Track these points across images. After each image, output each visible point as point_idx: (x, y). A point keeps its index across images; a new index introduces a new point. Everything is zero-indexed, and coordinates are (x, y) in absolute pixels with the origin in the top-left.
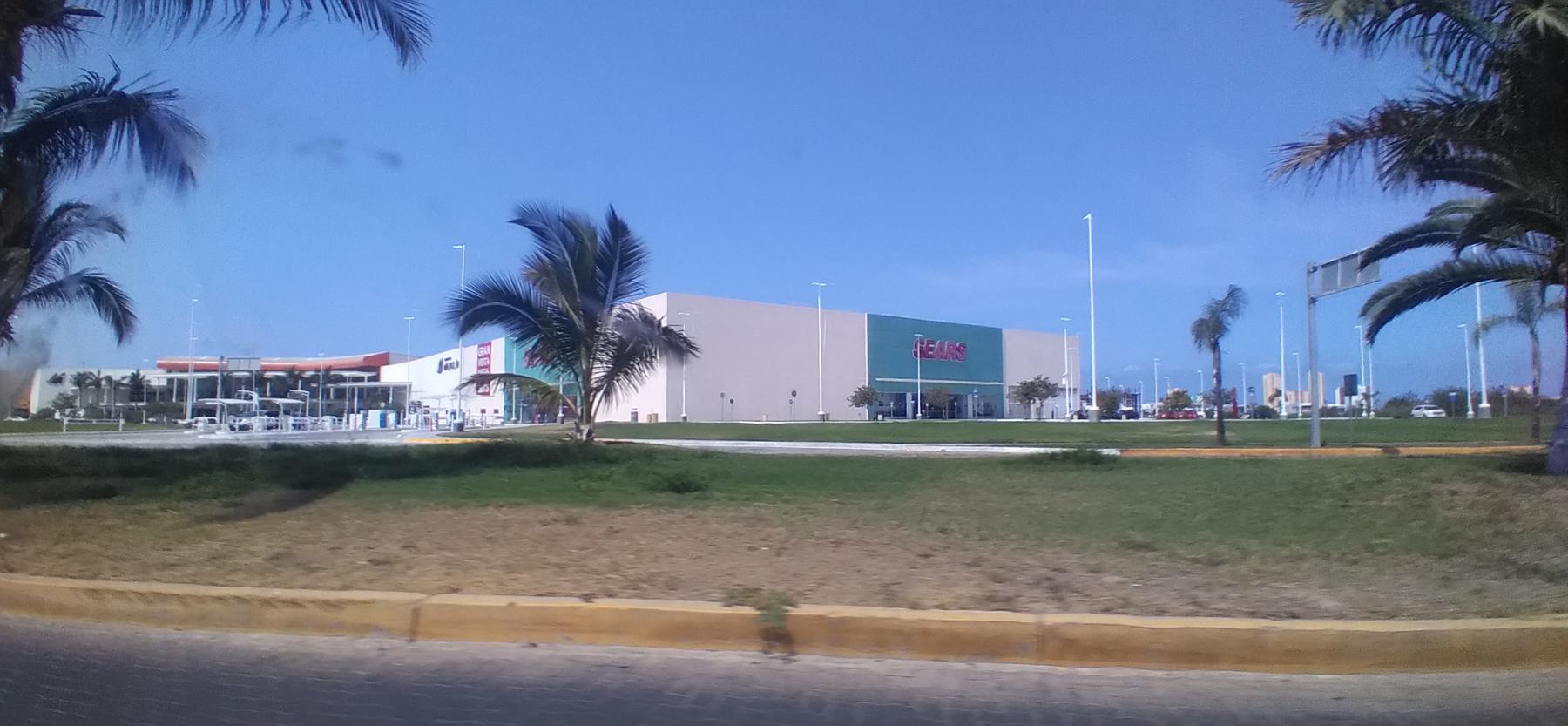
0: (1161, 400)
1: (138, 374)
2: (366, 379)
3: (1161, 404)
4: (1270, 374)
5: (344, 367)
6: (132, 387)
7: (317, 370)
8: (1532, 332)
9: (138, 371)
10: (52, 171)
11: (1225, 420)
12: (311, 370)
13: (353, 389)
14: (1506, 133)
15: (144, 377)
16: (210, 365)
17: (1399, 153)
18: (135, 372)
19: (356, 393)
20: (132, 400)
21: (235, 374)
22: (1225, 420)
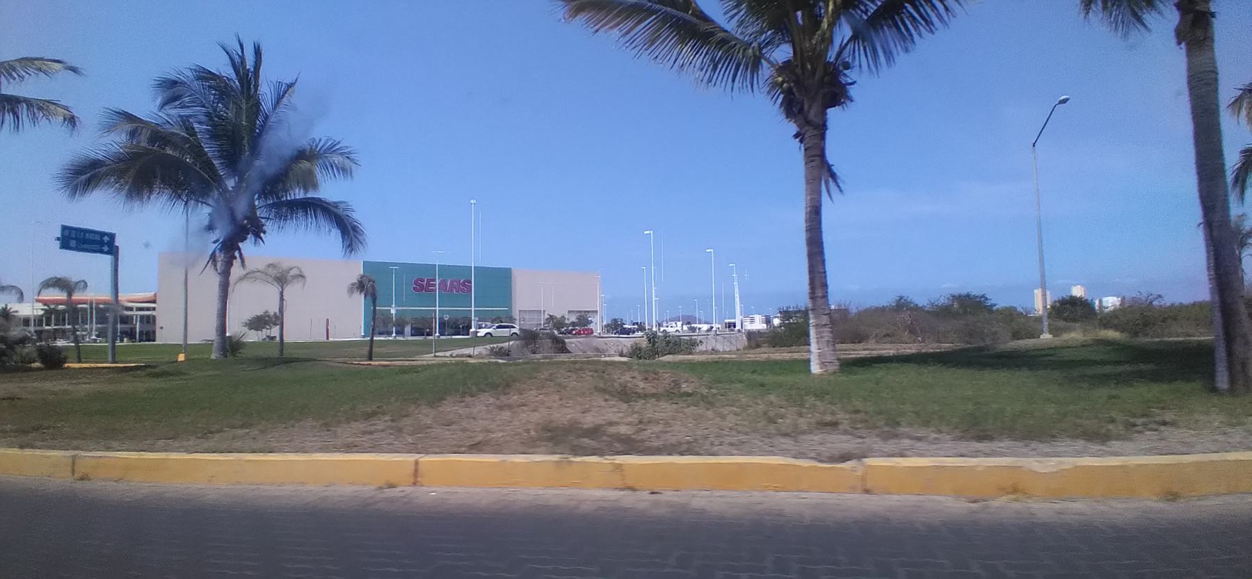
0: (96, 331)
1: (6, 308)
2: (135, 310)
3: (125, 340)
4: (803, 338)
5: (145, 300)
6: (1102, 312)
7: (91, 303)
8: (282, 294)
9: (6, 305)
10: (156, 153)
11: (73, 344)
12: (61, 304)
13: (137, 316)
14: (683, 22)
15: (11, 309)
16: (82, 300)
17: (674, 37)
18: (4, 306)
19: (139, 319)
20: (105, 327)
21: (80, 306)
22: (73, 344)
